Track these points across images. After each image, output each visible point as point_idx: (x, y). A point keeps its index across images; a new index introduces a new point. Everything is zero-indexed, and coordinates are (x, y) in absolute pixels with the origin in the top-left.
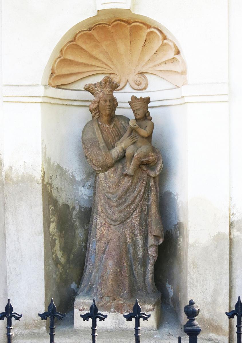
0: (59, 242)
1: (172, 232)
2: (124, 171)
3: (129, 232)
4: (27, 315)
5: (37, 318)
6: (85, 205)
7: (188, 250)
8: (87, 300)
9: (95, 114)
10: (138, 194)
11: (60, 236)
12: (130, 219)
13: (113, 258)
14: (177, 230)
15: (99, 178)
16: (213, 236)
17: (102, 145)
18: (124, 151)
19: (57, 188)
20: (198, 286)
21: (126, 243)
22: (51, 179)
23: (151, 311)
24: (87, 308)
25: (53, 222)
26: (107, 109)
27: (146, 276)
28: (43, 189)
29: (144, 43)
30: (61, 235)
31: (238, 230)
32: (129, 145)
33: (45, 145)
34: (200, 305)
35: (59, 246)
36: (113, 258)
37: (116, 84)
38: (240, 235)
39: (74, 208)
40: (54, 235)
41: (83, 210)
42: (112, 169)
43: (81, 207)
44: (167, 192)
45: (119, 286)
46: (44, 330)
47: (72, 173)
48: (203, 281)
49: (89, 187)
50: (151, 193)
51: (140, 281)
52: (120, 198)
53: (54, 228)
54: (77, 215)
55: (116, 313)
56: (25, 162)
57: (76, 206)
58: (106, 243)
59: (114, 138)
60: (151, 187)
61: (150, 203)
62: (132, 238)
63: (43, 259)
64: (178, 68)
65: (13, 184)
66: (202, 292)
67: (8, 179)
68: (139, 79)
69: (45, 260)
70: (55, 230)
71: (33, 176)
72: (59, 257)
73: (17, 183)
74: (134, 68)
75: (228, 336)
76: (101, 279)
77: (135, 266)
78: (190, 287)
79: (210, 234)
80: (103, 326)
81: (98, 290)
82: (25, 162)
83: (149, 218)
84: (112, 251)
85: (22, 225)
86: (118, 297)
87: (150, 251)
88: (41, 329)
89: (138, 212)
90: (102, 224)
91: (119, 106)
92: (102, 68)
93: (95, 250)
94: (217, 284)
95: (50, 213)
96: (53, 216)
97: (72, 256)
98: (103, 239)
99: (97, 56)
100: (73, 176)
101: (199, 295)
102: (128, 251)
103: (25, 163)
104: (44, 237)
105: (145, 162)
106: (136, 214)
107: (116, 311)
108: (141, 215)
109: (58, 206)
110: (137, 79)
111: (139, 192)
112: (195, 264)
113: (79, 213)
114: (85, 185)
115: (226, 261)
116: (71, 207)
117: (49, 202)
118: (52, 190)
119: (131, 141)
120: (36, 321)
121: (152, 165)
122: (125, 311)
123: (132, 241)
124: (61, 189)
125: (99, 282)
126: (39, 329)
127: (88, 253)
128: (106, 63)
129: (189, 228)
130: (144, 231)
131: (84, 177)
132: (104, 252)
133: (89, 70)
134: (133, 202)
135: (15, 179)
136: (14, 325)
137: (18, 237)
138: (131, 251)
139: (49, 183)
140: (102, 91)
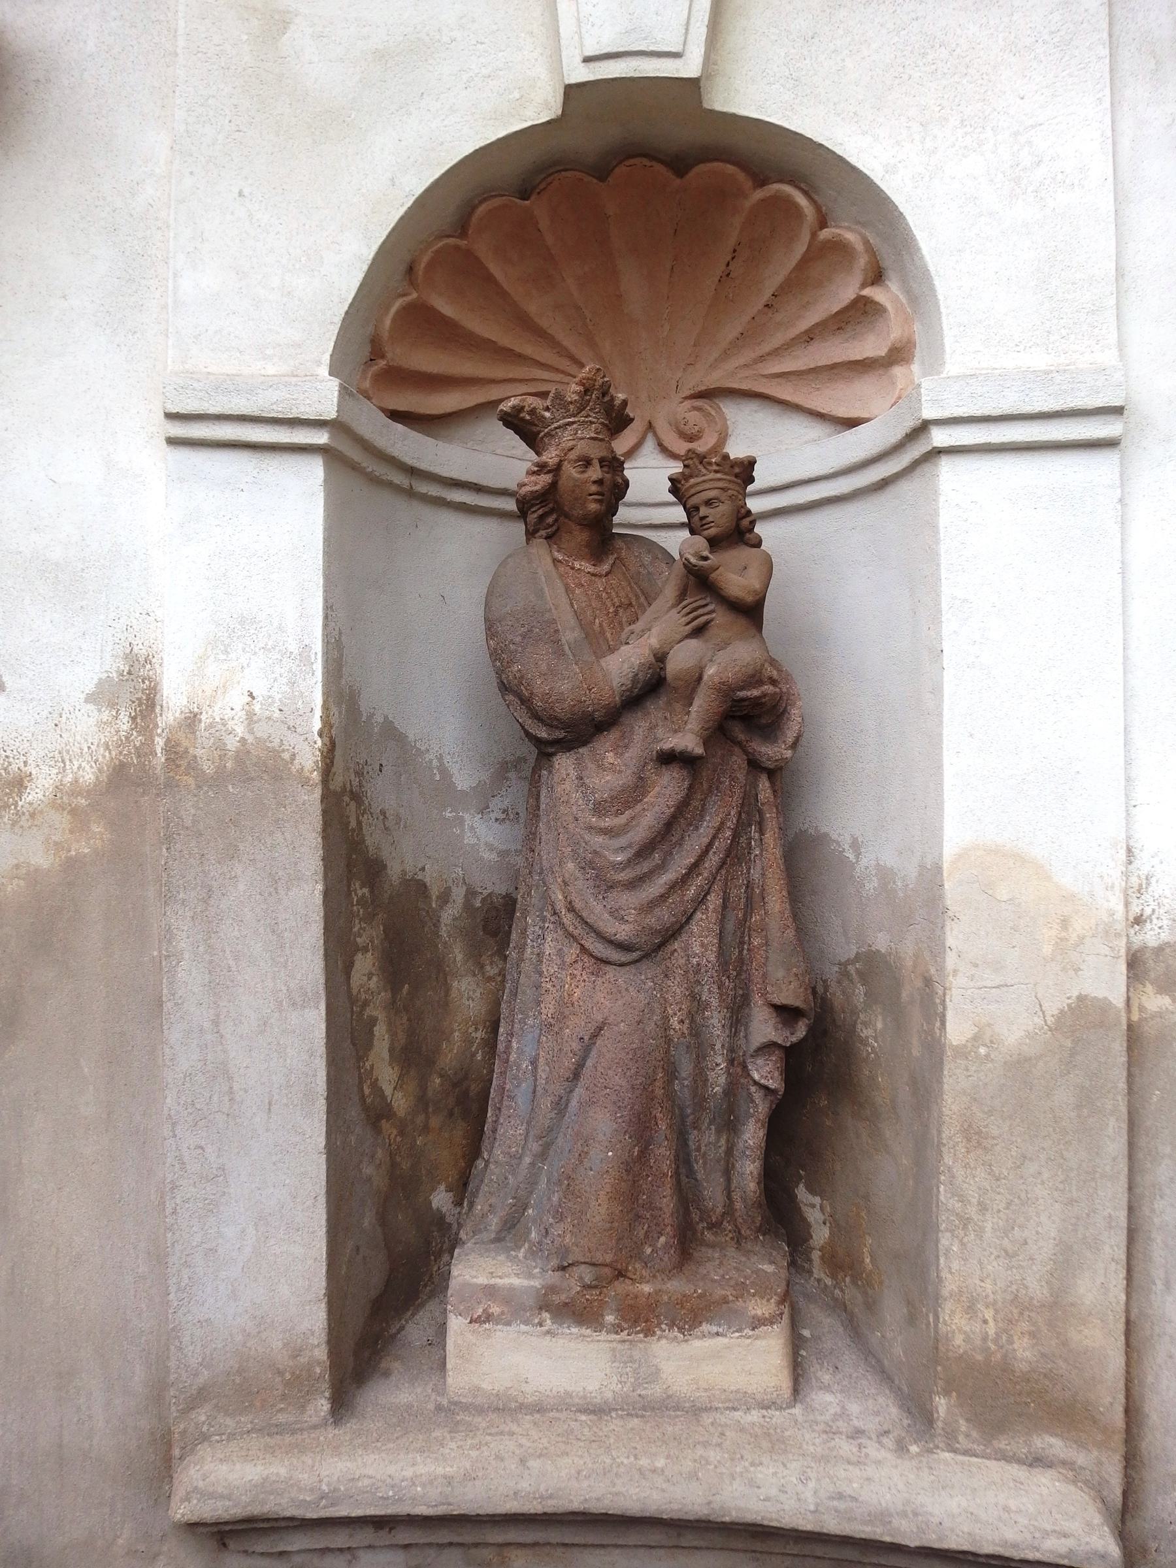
0: (389, 1031)
1: (826, 990)
2: (657, 740)
3: (678, 991)
4: (250, 1349)
5: (291, 1363)
6: (493, 885)
7: (945, 1072)
8: (501, 1277)
9: (542, 518)
10: (714, 837)
11: (392, 1006)
12: (684, 937)
13: (615, 1103)
14: (851, 981)
15: (550, 772)
16: (1056, 1012)
17: (570, 635)
18: (661, 658)
19: (383, 813)
20: (988, 1226)
21: (666, 1037)
22: (359, 774)
23: (772, 1323)
24: (503, 1313)
25: (365, 950)
26: (591, 495)
27: (733, 1165)
28: (325, 812)
29: (728, 265)
30: (394, 1002)
31: (1161, 990)
32: (678, 637)
33: (340, 633)
34: (997, 1311)
35: (386, 1045)
36: (615, 1103)
37: (624, 400)
38: (1170, 1008)
39: (445, 897)
40: (366, 1004)
41: (478, 903)
42: (613, 735)
43: (471, 893)
44: (803, 833)
45: (638, 1217)
46: (323, 1414)
47: (440, 758)
48: (1007, 1208)
49: (504, 816)
50: (761, 832)
51: (712, 1193)
52: (644, 851)
53: (370, 976)
54: (457, 923)
55: (626, 1332)
56: (251, 695)
57: (454, 889)
58: (586, 1038)
59: (616, 613)
60: (760, 812)
61: (755, 874)
62: (691, 1016)
63: (321, 1105)
64: (871, 346)
65: (199, 787)
66: (1006, 1252)
67: (178, 766)
68: (693, 417)
69: (328, 1112)
70: (373, 983)
71: (286, 756)
72: (388, 1090)
73: (219, 779)
74: (679, 374)
75: (1122, 1449)
76: (564, 1187)
77: (695, 1132)
78: (952, 1231)
79: (1041, 1006)
80: (570, 1389)
81: (547, 1232)
82: (251, 695)
83: (754, 934)
84: (610, 1073)
85: (232, 963)
86: (634, 1267)
87: (757, 1070)
88: (310, 1411)
89: (715, 910)
90: (568, 960)
91: (630, 496)
92: (557, 370)
93: (534, 1062)
94: (1073, 1221)
95: (352, 912)
96: (364, 925)
97: (438, 1081)
98: (573, 1021)
99: (544, 323)
100: (443, 770)
101: (990, 1267)
102: (672, 1073)
103: (253, 698)
104: (327, 1014)
105: (746, 703)
106: (704, 917)
107: (626, 1326)
108: (722, 921)
109: (386, 887)
110: (687, 415)
111: (719, 829)
112: (976, 1133)
113: (464, 914)
114: (488, 807)
115: (1112, 1122)
116: (434, 892)
117: (349, 865)
118: (364, 819)
119: (688, 624)
120: (288, 1376)
121: (763, 721)
122: (663, 1326)
123: (690, 1028)
124: (398, 818)
125: (555, 1199)
126: (303, 1408)
127: (502, 1074)
128: (574, 350)
129: (951, 978)
130: (735, 987)
131: (485, 776)
132: (575, 1074)
133: (511, 376)
134: (694, 868)
135: (208, 768)
136: (195, 1392)
137: (218, 1016)
138: (686, 1068)
139: (351, 791)
140: (573, 423)
